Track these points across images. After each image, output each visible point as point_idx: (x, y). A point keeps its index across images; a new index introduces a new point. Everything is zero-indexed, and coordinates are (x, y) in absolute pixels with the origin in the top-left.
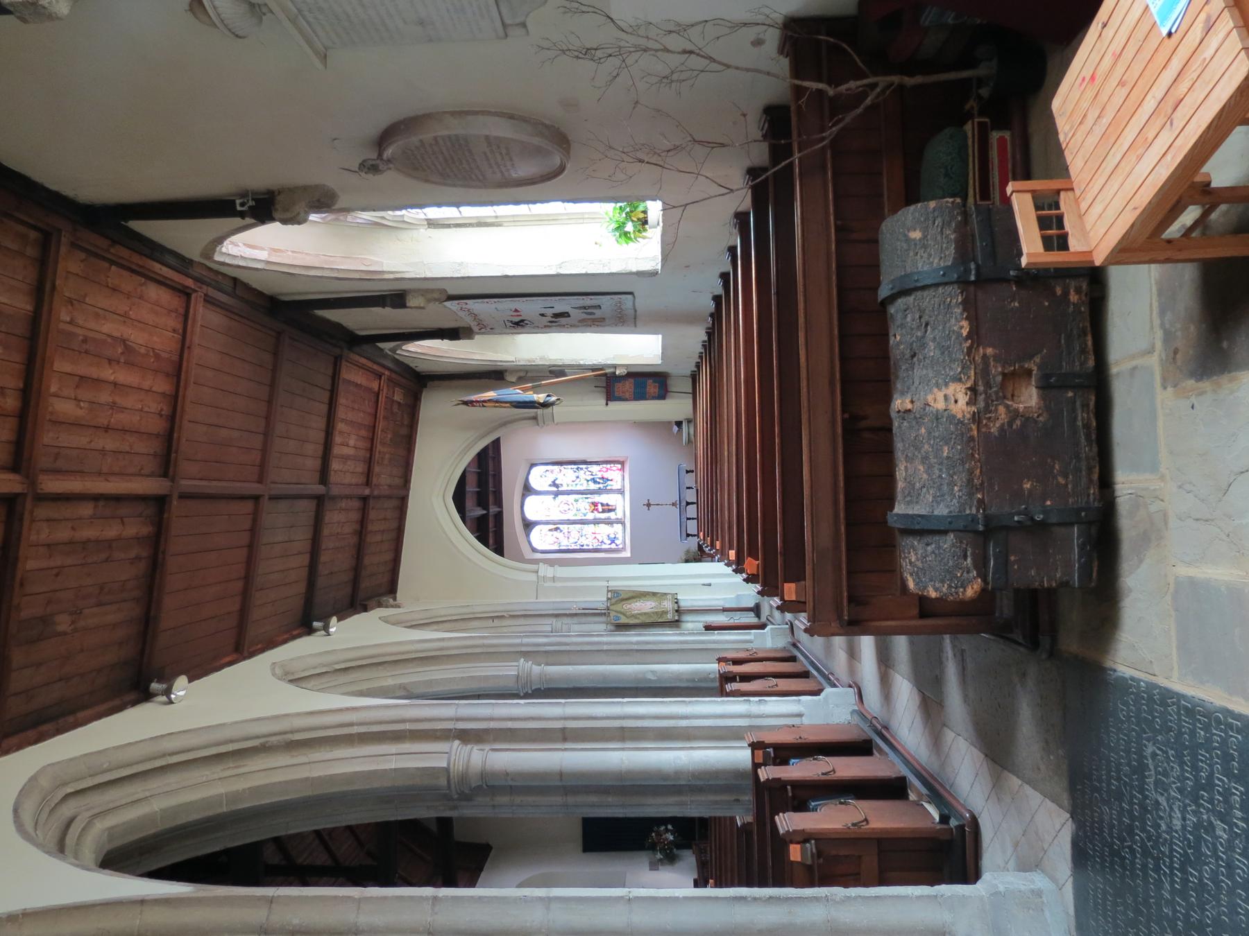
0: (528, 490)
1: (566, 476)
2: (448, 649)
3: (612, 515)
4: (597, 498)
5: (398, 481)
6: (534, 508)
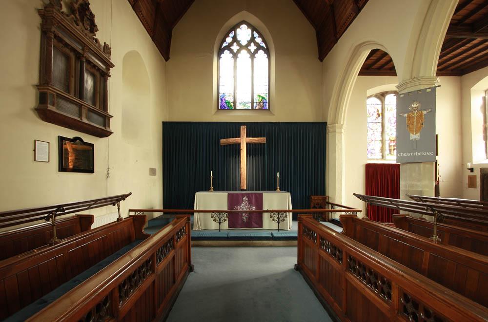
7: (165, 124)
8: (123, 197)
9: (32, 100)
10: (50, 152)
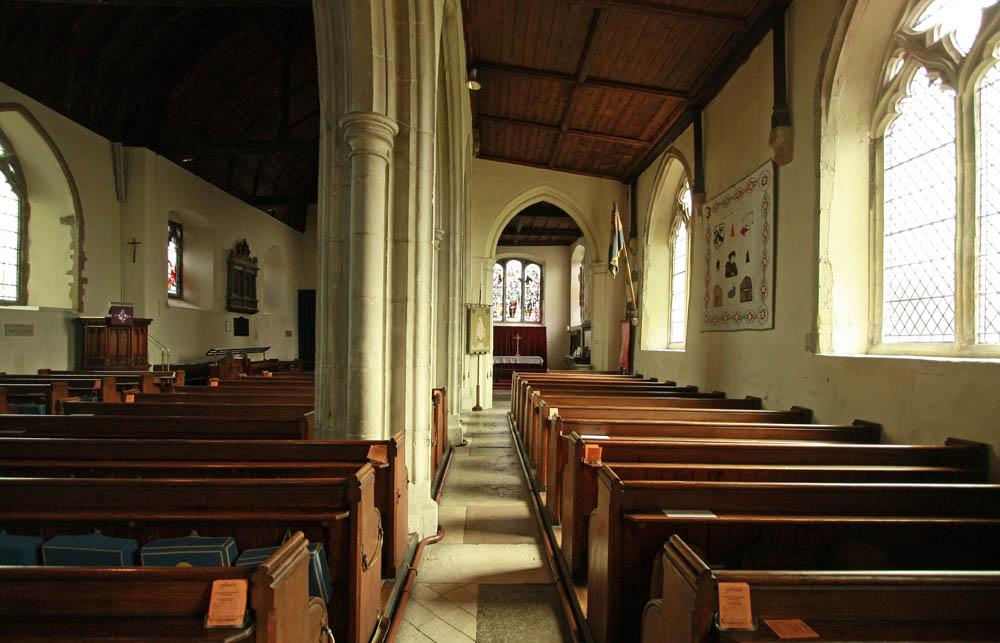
0: (525, 262)
1: (534, 287)
2: (454, 175)
3: (508, 315)
4: (518, 306)
5: (559, 163)
6: (514, 266)
7: (299, 291)
8: (267, 349)
9: (224, 303)
10: (231, 327)
